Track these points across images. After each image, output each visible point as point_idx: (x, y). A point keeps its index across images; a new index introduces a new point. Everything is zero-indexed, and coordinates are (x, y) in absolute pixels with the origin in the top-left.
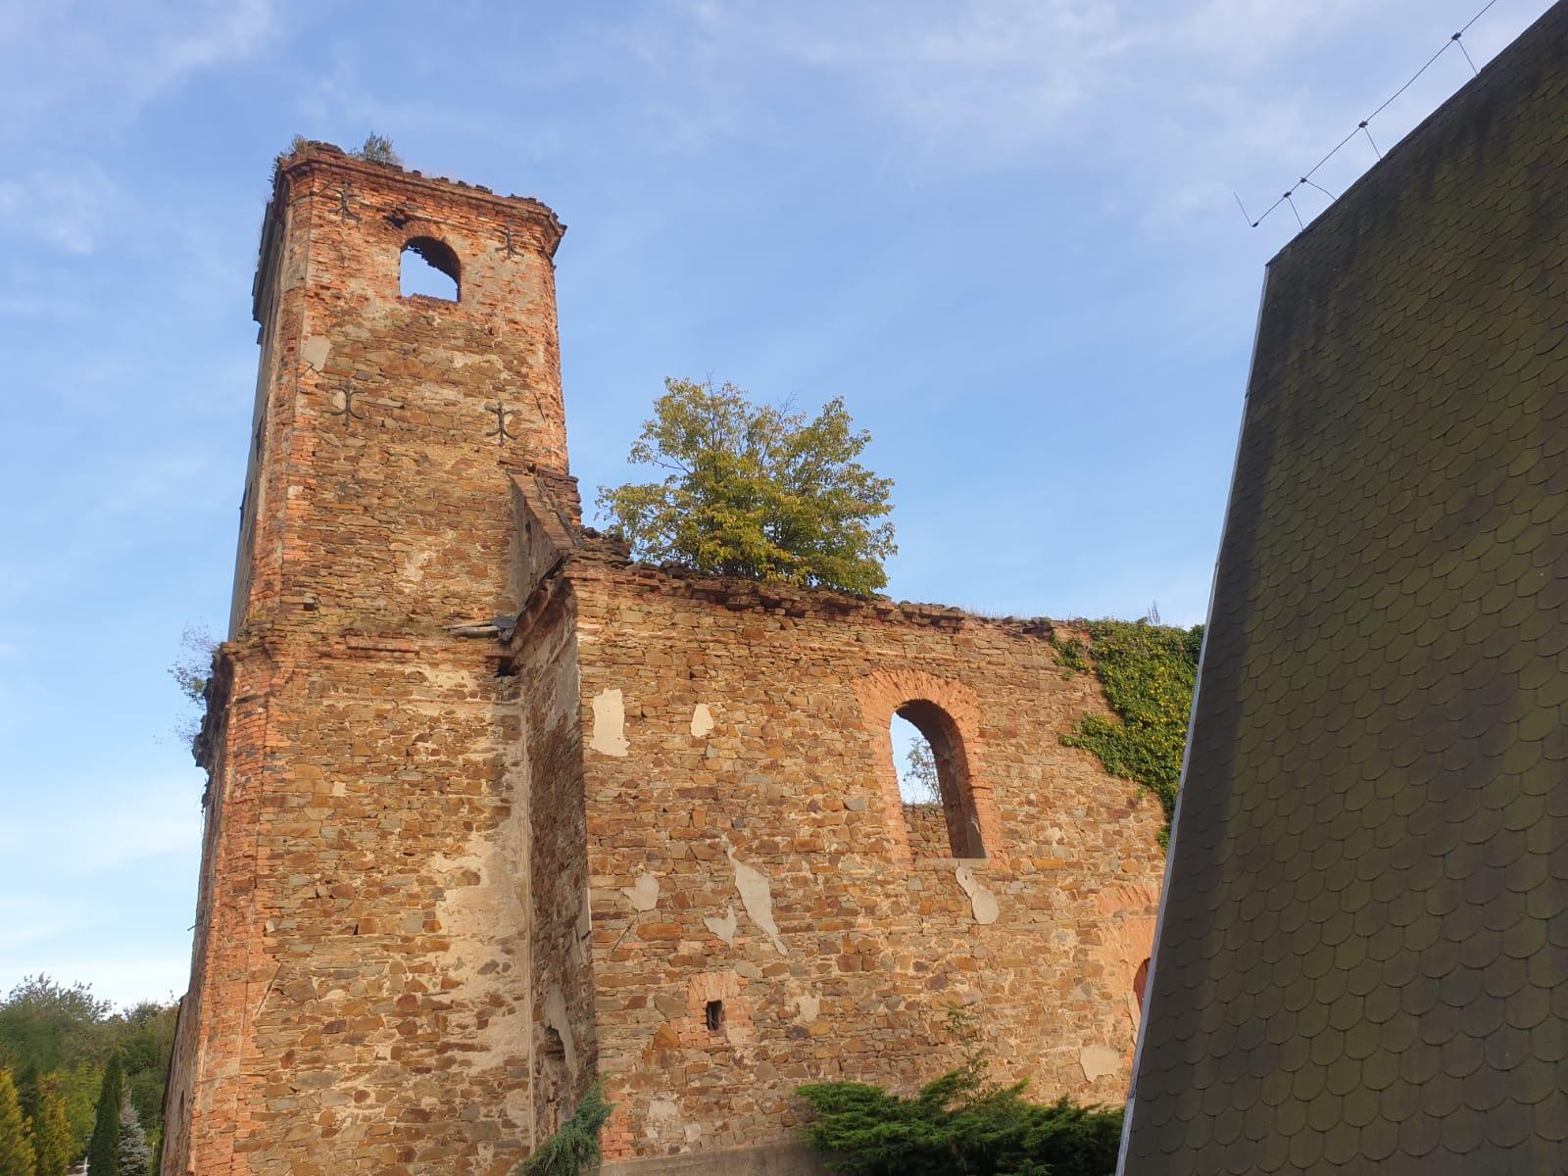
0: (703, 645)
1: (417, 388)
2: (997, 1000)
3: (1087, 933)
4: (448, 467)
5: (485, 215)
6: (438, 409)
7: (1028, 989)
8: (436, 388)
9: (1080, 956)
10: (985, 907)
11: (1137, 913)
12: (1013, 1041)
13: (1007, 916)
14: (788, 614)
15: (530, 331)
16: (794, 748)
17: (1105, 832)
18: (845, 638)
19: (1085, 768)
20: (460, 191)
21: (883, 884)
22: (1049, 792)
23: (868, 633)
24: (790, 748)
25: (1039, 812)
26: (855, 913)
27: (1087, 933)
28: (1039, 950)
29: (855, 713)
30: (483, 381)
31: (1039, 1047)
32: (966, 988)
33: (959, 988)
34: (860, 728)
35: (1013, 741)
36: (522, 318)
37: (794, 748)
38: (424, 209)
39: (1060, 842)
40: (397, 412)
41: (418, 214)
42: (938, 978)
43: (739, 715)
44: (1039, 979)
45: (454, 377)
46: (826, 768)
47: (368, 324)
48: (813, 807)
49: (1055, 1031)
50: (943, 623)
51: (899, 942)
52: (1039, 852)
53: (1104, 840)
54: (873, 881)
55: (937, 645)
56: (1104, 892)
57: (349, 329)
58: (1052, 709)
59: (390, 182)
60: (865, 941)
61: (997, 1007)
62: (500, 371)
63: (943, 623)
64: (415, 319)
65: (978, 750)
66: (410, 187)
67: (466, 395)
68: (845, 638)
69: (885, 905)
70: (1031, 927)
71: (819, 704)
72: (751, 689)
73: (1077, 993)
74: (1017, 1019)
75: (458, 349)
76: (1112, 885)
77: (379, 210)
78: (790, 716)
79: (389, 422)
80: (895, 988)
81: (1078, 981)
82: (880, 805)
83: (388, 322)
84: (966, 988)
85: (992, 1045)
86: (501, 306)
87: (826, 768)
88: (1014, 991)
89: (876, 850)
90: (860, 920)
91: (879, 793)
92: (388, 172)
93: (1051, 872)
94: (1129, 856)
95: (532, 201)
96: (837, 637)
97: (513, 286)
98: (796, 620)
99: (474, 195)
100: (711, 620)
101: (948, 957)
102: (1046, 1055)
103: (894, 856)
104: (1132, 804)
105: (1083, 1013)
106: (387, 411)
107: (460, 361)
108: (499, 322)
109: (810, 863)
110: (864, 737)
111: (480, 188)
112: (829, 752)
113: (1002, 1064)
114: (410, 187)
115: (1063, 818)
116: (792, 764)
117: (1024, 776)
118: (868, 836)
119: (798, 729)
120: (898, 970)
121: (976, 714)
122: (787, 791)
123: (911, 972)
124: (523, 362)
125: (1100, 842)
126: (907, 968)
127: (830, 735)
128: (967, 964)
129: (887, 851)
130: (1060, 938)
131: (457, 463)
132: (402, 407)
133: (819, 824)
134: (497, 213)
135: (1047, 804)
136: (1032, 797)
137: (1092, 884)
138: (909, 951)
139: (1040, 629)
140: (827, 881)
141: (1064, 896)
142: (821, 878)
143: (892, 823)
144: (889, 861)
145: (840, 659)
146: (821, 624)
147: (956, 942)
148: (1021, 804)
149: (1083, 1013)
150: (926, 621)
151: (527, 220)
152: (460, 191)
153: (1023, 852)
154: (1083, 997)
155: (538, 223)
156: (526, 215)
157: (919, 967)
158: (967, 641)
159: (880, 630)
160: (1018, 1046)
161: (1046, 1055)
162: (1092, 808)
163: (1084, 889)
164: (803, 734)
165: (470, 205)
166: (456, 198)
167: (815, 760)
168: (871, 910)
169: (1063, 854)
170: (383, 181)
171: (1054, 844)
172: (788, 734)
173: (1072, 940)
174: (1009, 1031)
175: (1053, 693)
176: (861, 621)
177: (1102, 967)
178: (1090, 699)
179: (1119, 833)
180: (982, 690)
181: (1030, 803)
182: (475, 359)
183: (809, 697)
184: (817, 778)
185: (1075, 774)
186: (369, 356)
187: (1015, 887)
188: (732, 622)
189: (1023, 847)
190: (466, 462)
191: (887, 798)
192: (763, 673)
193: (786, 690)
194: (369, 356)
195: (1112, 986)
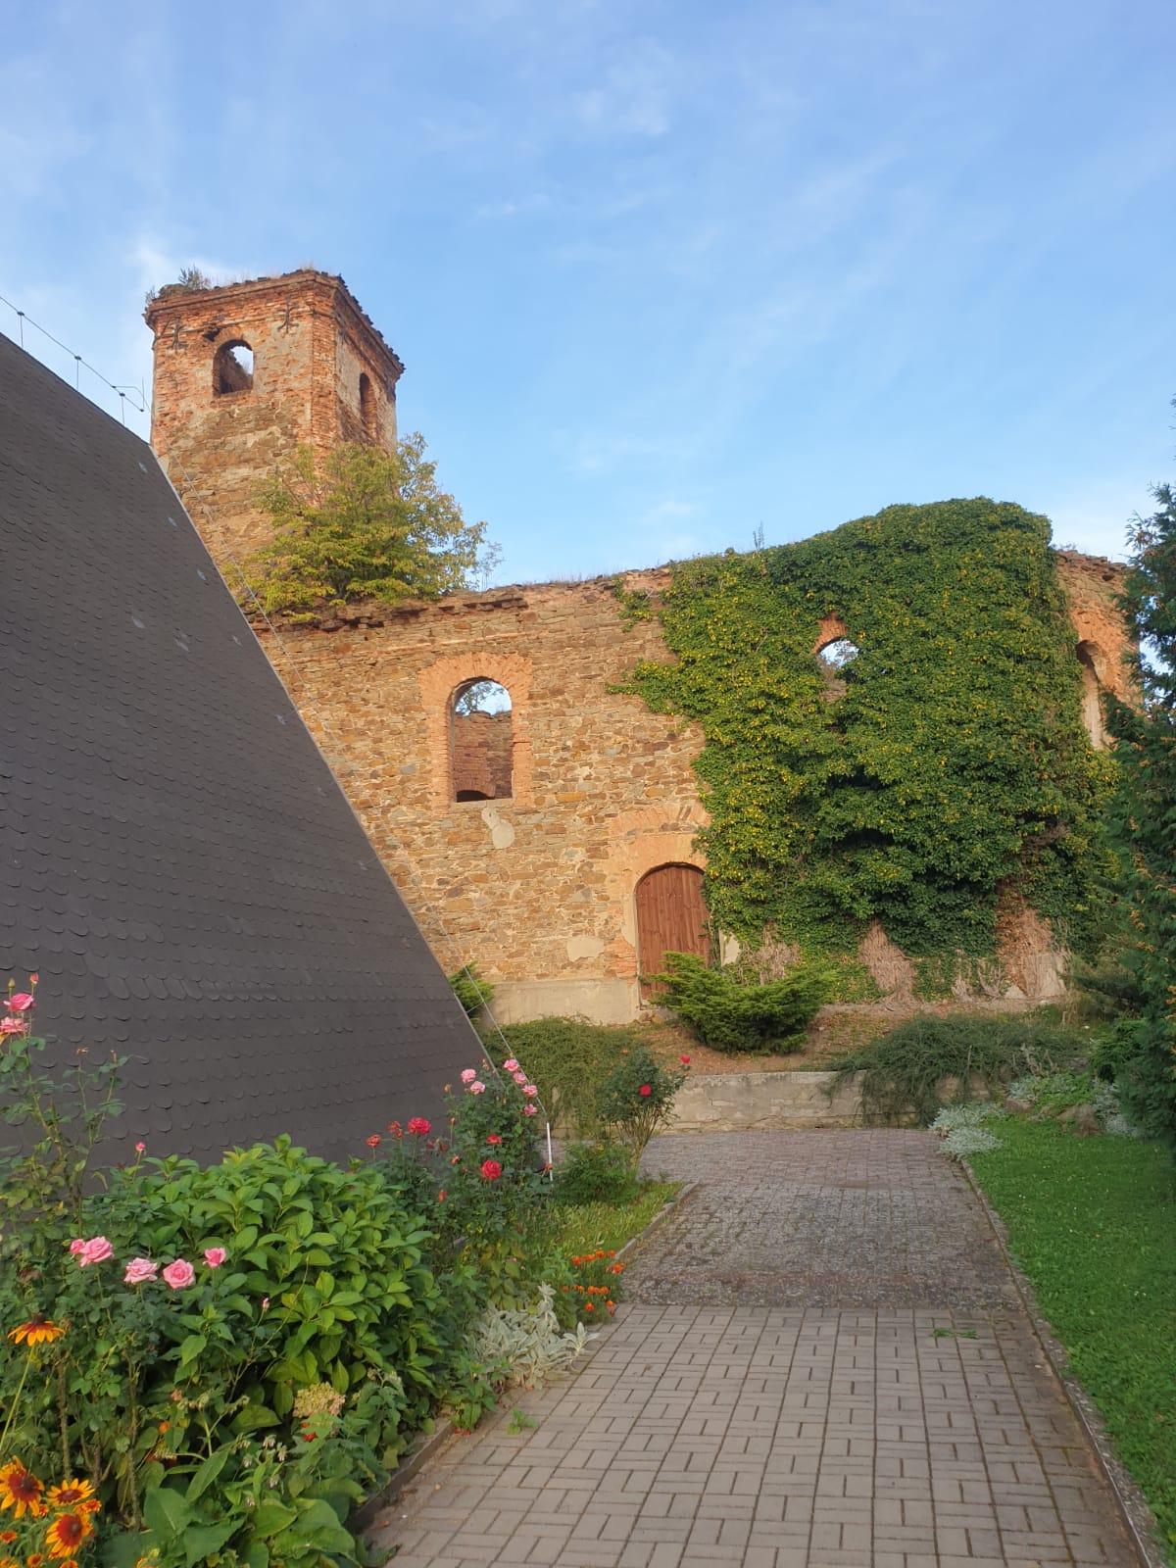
0: (303, 666)
1: (223, 474)
2: (503, 903)
3: (596, 851)
4: (242, 533)
5: (270, 300)
6: (237, 486)
7: (533, 894)
8: (235, 470)
9: (586, 868)
10: (501, 835)
11: (651, 831)
12: (509, 932)
13: (522, 842)
14: (370, 626)
15: (301, 394)
16: (365, 734)
17: (638, 765)
18: (419, 635)
19: (631, 713)
20: (248, 289)
21: (420, 825)
22: (586, 739)
23: (438, 627)
24: (362, 733)
25: (573, 756)
26: (395, 847)
27: (596, 851)
28: (548, 865)
29: (417, 698)
30: (266, 452)
31: (533, 936)
32: (477, 895)
33: (472, 895)
34: (420, 710)
35: (560, 698)
36: (295, 385)
37: (365, 734)
38: (228, 315)
39: (588, 778)
40: (210, 499)
41: (226, 323)
42: (456, 889)
43: (326, 714)
44: (543, 886)
45: (247, 456)
46: (389, 747)
47: (192, 434)
48: (374, 775)
49: (549, 924)
50: (504, 605)
51: (428, 866)
52: (564, 788)
53: (633, 772)
54: (413, 824)
55: (502, 624)
56: (621, 815)
57: (181, 443)
58: (608, 662)
59: (204, 304)
60: (401, 866)
61: (501, 908)
62: (278, 439)
63: (504, 605)
64: (222, 416)
65: (523, 712)
66: (217, 302)
67: (255, 468)
68: (419, 635)
69: (420, 840)
70: (543, 848)
71: (388, 695)
72: (335, 695)
73: (577, 897)
74: (518, 917)
75: (251, 431)
76: (631, 809)
77: (199, 331)
78: (364, 709)
79: (206, 508)
80: (420, 897)
81: (580, 887)
82: (429, 767)
83: (206, 427)
84: (477, 895)
85: (493, 935)
86: (281, 379)
87: (389, 747)
88: (517, 896)
89: (421, 800)
90: (399, 852)
91: (429, 759)
92: (198, 297)
93: (571, 804)
94: (657, 783)
95: (299, 272)
96: (412, 637)
97: (290, 357)
98: (378, 630)
99: (246, 290)
100: (310, 644)
101: (466, 874)
102: (536, 942)
103: (433, 804)
104: (672, 737)
105: (579, 911)
106: (204, 499)
107: (251, 440)
108: (280, 397)
109: (367, 814)
110: (423, 715)
111: (261, 280)
112: (392, 733)
113: (498, 948)
114: (217, 302)
115: (595, 757)
116: (362, 746)
117: (563, 726)
118: (416, 791)
119: (369, 718)
120: (424, 885)
121: (529, 680)
122: (356, 766)
123: (435, 885)
124: (295, 423)
125: (629, 774)
126: (432, 883)
127: (395, 720)
128: (481, 879)
129: (429, 801)
130: (571, 855)
131: (248, 526)
132: (214, 494)
133: (377, 787)
134: (279, 294)
135: (582, 747)
136: (569, 743)
137: (611, 809)
138: (436, 871)
139: (611, 586)
140: (377, 826)
141: (580, 822)
142: (373, 825)
143: (435, 780)
144: (428, 808)
145: (411, 655)
146: (398, 628)
147: (474, 863)
148: (556, 751)
149: (579, 911)
150: (488, 607)
151: (302, 290)
152: (248, 289)
153: (548, 790)
154: (583, 899)
155: (310, 289)
156: (298, 286)
157: (441, 882)
158: (532, 615)
159: (450, 622)
160: (513, 936)
161: (536, 942)
162: (627, 746)
163: (602, 814)
164: (372, 722)
165: (260, 297)
166: (247, 296)
167: (380, 740)
168: (407, 845)
169: (587, 788)
170: (198, 305)
171: (581, 781)
172: (361, 723)
173: (580, 855)
174: (509, 925)
175: (609, 646)
176: (432, 619)
177: (605, 876)
178: (648, 645)
179: (652, 764)
180: (538, 658)
181: (565, 748)
182: (262, 434)
183: (379, 690)
184: (380, 754)
185: (617, 717)
186: (193, 460)
187: (535, 818)
188: (325, 643)
189: (550, 786)
190: (254, 524)
191: (435, 761)
192: (346, 679)
193: (362, 689)
194: (193, 460)
195: (610, 890)
